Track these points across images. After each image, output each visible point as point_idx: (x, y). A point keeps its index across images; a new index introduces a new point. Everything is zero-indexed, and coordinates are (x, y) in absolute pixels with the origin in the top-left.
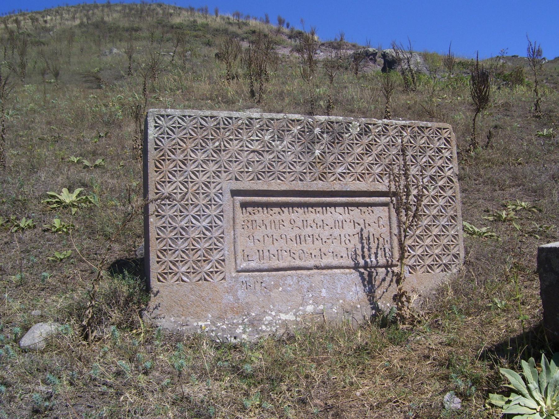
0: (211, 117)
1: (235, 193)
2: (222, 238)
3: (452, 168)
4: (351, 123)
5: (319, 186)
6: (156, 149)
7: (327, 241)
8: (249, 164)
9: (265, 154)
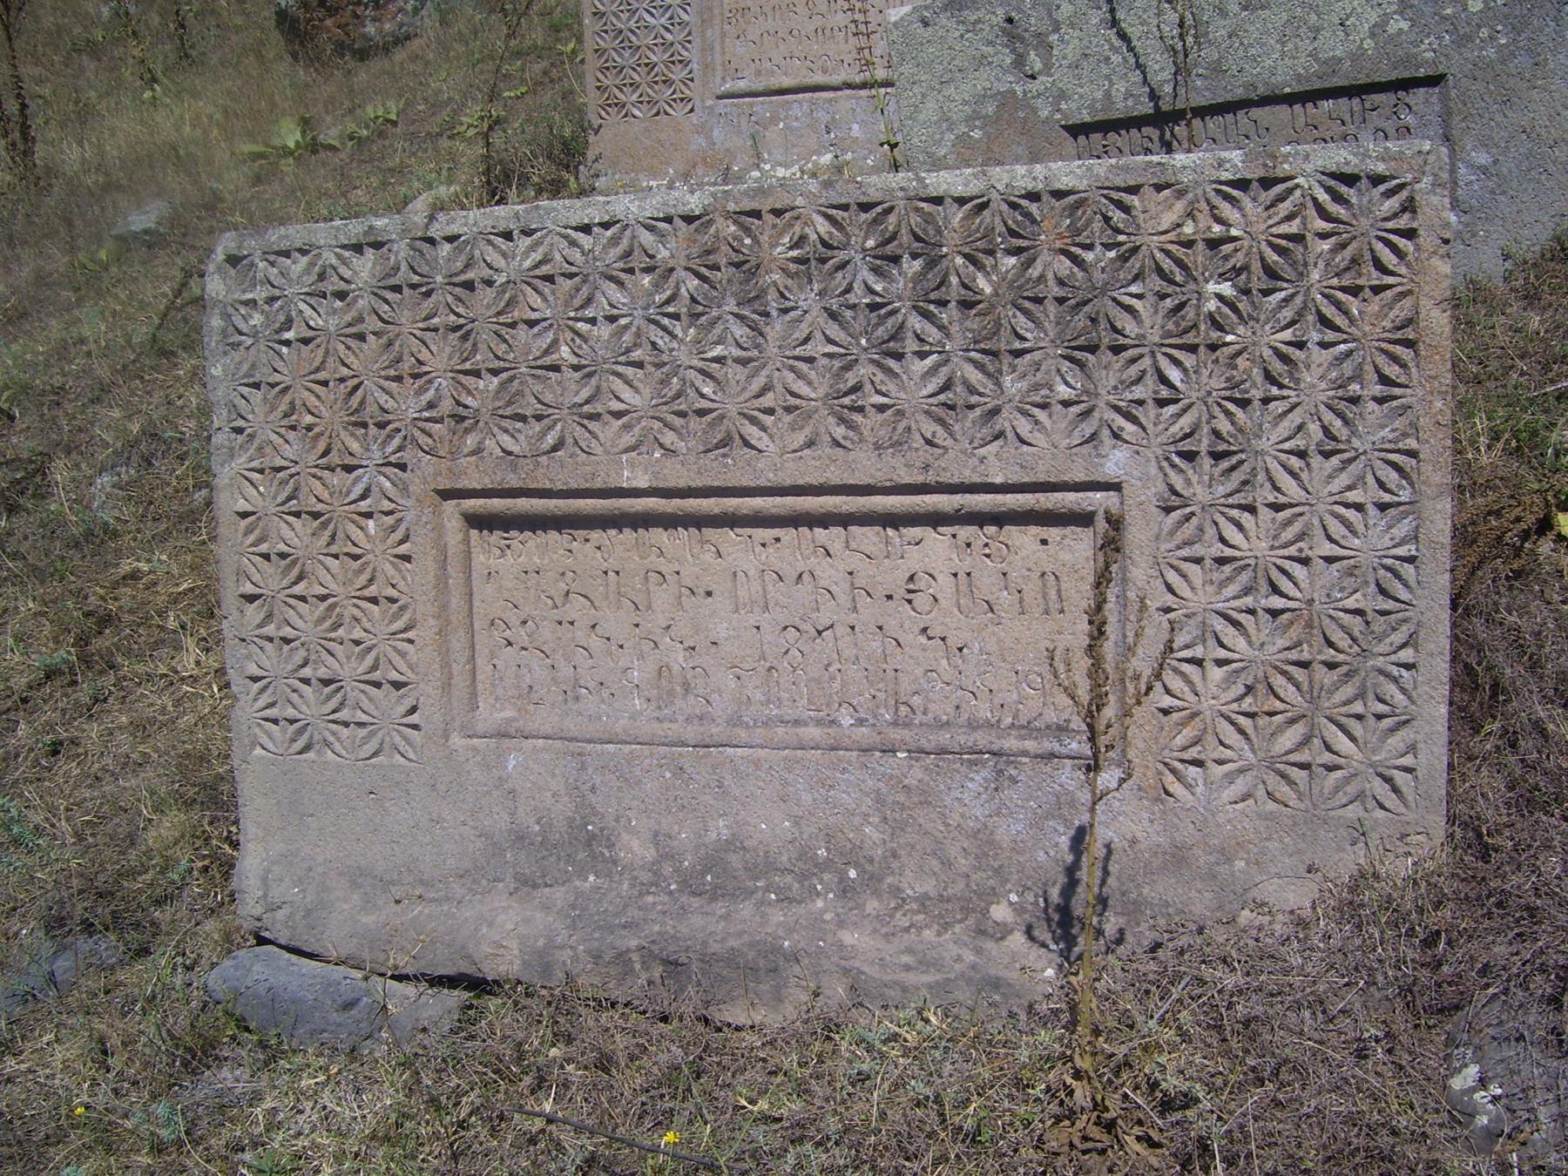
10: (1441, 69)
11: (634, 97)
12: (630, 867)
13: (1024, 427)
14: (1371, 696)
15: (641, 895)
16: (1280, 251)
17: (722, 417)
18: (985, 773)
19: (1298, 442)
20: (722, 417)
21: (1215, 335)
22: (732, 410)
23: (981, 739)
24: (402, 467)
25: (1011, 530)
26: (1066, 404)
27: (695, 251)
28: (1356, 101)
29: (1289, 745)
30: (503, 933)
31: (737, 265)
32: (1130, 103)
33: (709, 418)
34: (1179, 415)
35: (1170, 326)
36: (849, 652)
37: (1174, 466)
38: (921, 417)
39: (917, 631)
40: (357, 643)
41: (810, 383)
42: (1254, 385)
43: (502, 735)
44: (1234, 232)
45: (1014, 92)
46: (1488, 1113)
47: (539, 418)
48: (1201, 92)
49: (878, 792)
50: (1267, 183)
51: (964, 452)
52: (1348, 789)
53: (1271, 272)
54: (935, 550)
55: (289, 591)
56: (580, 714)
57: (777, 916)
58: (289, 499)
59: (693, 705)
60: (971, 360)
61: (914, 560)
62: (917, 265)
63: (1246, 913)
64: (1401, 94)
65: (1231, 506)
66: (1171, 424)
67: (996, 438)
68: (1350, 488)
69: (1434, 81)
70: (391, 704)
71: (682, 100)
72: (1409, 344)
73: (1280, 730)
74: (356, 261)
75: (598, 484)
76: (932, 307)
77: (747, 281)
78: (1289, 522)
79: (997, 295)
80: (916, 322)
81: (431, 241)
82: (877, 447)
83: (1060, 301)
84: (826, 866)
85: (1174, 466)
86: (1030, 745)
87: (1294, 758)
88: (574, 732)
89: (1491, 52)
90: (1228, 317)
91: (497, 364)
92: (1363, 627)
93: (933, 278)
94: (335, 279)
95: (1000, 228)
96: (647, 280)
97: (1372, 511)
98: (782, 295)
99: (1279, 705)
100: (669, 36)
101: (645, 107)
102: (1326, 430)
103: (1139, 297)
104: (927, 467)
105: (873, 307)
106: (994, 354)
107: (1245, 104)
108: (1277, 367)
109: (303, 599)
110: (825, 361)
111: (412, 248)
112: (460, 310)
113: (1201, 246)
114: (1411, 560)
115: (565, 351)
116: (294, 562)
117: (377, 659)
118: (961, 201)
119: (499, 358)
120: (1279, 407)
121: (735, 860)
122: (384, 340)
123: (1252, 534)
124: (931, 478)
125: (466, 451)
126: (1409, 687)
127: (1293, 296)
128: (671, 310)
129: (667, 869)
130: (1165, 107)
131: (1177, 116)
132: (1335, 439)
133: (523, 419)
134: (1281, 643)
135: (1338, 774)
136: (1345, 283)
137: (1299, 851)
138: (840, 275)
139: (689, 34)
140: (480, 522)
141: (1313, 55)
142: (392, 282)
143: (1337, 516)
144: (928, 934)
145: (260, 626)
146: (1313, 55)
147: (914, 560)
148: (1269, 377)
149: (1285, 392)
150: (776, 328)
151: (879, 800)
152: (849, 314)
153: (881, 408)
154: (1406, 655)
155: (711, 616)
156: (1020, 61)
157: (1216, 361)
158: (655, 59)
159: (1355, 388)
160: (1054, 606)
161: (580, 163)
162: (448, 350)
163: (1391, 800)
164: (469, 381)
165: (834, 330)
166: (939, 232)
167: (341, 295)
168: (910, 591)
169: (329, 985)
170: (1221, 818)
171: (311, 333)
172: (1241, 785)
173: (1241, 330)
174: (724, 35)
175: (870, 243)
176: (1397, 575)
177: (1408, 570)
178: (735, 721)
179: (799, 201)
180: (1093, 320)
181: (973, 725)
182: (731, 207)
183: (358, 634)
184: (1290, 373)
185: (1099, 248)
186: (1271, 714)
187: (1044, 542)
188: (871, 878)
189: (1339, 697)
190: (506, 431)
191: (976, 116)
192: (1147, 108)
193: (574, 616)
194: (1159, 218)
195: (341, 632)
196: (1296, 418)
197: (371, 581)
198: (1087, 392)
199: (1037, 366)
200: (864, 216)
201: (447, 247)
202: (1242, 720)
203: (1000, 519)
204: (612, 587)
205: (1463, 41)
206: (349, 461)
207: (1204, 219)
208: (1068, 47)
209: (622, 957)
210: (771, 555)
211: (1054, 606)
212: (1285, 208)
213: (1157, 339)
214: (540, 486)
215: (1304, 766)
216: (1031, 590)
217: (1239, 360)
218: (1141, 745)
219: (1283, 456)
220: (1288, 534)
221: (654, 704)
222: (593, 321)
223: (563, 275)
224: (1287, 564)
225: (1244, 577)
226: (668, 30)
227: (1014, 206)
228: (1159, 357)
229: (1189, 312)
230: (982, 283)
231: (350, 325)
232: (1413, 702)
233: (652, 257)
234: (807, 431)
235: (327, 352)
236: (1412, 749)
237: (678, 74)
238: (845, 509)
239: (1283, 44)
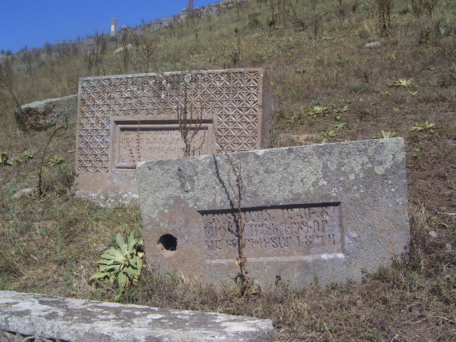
0: (108, 79)
1: (117, 123)
2: (108, 148)
3: (257, 101)
4: (186, 75)
5: (162, 117)
6: (82, 100)
7: (167, 152)
8: (125, 105)
10: (339, 200)
28: (307, 209)
32: (222, 204)
45: (180, 197)
48: (244, 204)
64: (324, 208)
69: (336, 204)
71: (105, 167)
89: (357, 195)
100: (102, 146)
107: (265, 208)
130: (235, 207)
131: (237, 211)
139: (109, 146)
141: (291, 191)
146: (291, 191)
156: (183, 185)
158: (97, 153)
161: (72, 185)
174: (120, 147)
191: (166, 204)
192: (228, 207)
208: (200, 182)
226: (102, 143)
237: (104, 159)
239: (280, 187)
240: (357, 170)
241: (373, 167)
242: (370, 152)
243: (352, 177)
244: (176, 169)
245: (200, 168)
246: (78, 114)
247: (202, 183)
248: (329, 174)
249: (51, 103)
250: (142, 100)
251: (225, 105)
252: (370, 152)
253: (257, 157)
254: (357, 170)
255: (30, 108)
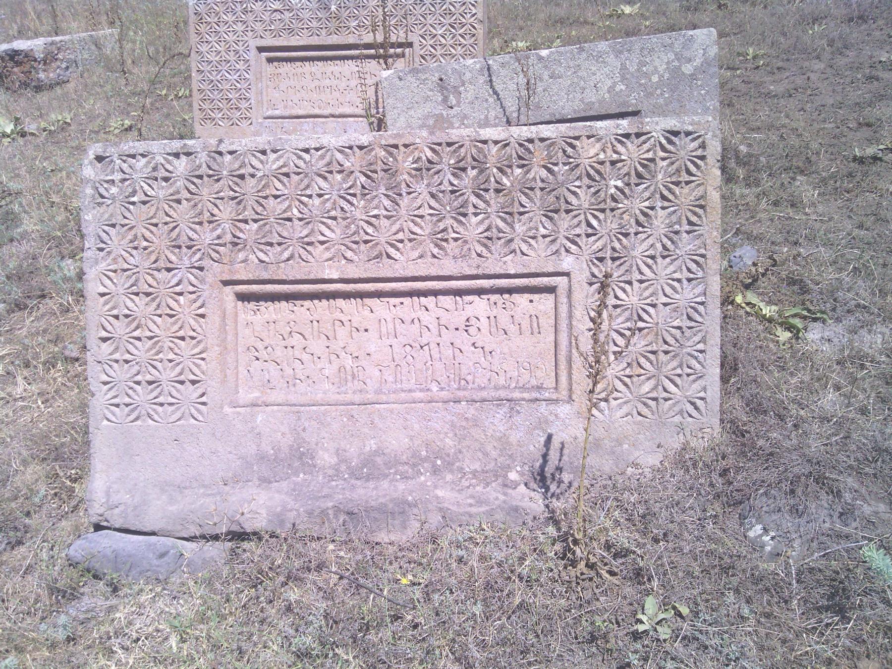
1: (261, 49)
5: (334, 40)
6: (196, 14)
9: (286, 13)
10: (639, 108)
11: (220, 115)
12: (323, 468)
13: (524, 247)
14: (685, 366)
15: (329, 481)
16: (644, 166)
17: (377, 244)
18: (505, 409)
19: (651, 252)
20: (377, 244)
21: (613, 204)
22: (383, 240)
23: (503, 394)
24: (201, 269)
25: (516, 297)
26: (544, 237)
27: (364, 163)
29: (647, 390)
30: (258, 506)
31: (385, 171)
33: (370, 244)
34: (597, 241)
35: (593, 200)
36: (436, 356)
37: (594, 264)
38: (476, 244)
39: (470, 344)
40: (170, 361)
41: (421, 228)
42: (631, 226)
43: (254, 405)
44: (623, 157)
45: (442, 114)
46: (770, 545)
47: (280, 244)
49: (452, 421)
50: (638, 135)
51: (496, 259)
52: (675, 409)
53: (639, 176)
54: (479, 306)
55: (130, 335)
56: (296, 393)
57: (401, 486)
58: (132, 286)
59: (358, 385)
60: (500, 217)
61: (469, 311)
62: (475, 172)
63: (630, 469)
65: (620, 282)
66: (591, 246)
67: (511, 253)
68: (675, 272)
70: (191, 392)
72: (702, 207)
73: (643, 383)
74: (176, 162)
75: (312, 277)
76: (481, 192)
77: (391, 179)
78: (647, 288)
79: (513, 186)
80: (474, 199)
81: (220, 153)
82: (454, 258)
83: (542, 189)
84: (426, 459)
85: (594, 264)
86: (526, 395)
87: (649, 395)
88: (294, 401)
89: (661, 101)
90: (618, 196)
91: (257, 217)
92: (680, 334)
93: (482, 178)
94: (163, 170)
95: (515, 155)
96: (339, 177)
97: (685, 282)
98: (408, 186)
99: (643, 372)
101: (226, 121)
102: (664, 247)
103: (579, 187)
104: (478, 267)
105: (453, 192)
106: (511, 214)
108: (642, 218)
109: (139, 339)
110: (428, 217)
111: (209, 156)
112: (237, 189)
113: (608, 164)
114: (702, 303)
115: (295, 211)
116: (134, 320)
117: (183, 369)
118: (496, 142)
119: (258, 214)
120: (643, 236)
121: (379, 460)
122: (192, 203)
123: (630, 294)
124: (480, 272)
125: (239, 260)
126: (702, 360)
127: (649, 186)
128: (351, 191)
129: (343, 467)
132: (668, 250)
133: (271, 244)
134: (643, 343)
135: (670, 402)
136: (674, 180)
137: (653, 439)
138: (436, 176)
140: (243, 297)
141: (582, 100)
142: (197, 173)
143: (668, 285)
144: (478, 488)
145: (110, 354)
146: (582, 100)
147: (469, 311)
148: (638, 223)
149: (646, 230)
150: (405, 202)
151: (453, 425)
152: (441, 195)
153: (456, 240)
154: (701, 346)
155: (367, 341)
156: (445, 99)
157: (614, 216)
158: (231, 96)
159: (677, 227)
160: (536, 330)
162: (229, 209)
163: (694, 413)
164: (242, 225)
165: (433, 203)
166: (485, 157)
167: (166, 179)
168: (466, 326)
169: (150, 545)
170: (617, 425)
171: (148, 199)
172: (625, 409)
173: (626, 202)
175: (452, 162)
176: (696, 310)
177: (701, 308)
178: (378, 392)
179: (418, 141)
180: (557, 198)
181: (496, 388)
182: (383, 142)
183: (171, 356)
184: (648, 221)
185: (561, 165)
186: (639, 376)
187: (531, 301)
188: (449, 464)
189: (670, 367)
190: (262, 251)
193: (294, 343)
194: (589, 151)
195: (161, 355)
196: (650, 241)
197: (181, 328)
198: (554, 231)
199: (531, 219)
200: (448, 149)
201: (229, 156)
202: (626, 379)
203: (510, 291)
204: (316, 328)
205: (649, 95)
206: (169, 265)
207: (609, 152)
208: (469, 93)
209: (324, 512)
210: (400, 312)
211: (536, 330)
212: (646, 146)
213: (587, 206)
214: (280, 278)
215: (655, 399)
216: (525, 324)
217: (624, 216)
218: (579, 393)
219: (644, 258)
220: (647, 293)
221: (336, 386)
222: (310, 196)
223: (294, 173)
224: (646, 307)
225: (627, 313)
227: (521, 145)
228: (588, 214)
229: (602, 194)
230: (505, 180)
231: (172, 195)
232: (704, 367)
233: (342, 165)
234: (419, 251)
235: (158, 208)
236: (704, 389)
237: (244, 105)
238: (437, 287)
240: (662, 68)
241: (680, 66)
242: (677, 47)
243: (655, 79)
244: (435, 79)
245: (468, 75)
246: (192, 37)
247: (470, 96)
248: (628, 76)
249: (52, 43)
250: (300, 14)
251: (430, 20)
252: (677, 47)
253: (541, 58)
254: (662, 68)
255: (16, 51)
